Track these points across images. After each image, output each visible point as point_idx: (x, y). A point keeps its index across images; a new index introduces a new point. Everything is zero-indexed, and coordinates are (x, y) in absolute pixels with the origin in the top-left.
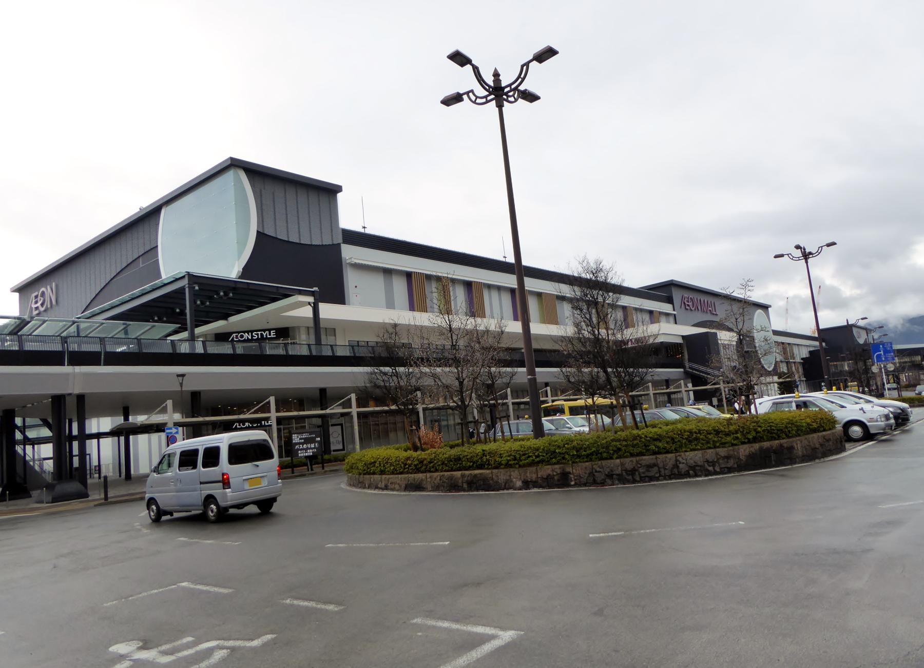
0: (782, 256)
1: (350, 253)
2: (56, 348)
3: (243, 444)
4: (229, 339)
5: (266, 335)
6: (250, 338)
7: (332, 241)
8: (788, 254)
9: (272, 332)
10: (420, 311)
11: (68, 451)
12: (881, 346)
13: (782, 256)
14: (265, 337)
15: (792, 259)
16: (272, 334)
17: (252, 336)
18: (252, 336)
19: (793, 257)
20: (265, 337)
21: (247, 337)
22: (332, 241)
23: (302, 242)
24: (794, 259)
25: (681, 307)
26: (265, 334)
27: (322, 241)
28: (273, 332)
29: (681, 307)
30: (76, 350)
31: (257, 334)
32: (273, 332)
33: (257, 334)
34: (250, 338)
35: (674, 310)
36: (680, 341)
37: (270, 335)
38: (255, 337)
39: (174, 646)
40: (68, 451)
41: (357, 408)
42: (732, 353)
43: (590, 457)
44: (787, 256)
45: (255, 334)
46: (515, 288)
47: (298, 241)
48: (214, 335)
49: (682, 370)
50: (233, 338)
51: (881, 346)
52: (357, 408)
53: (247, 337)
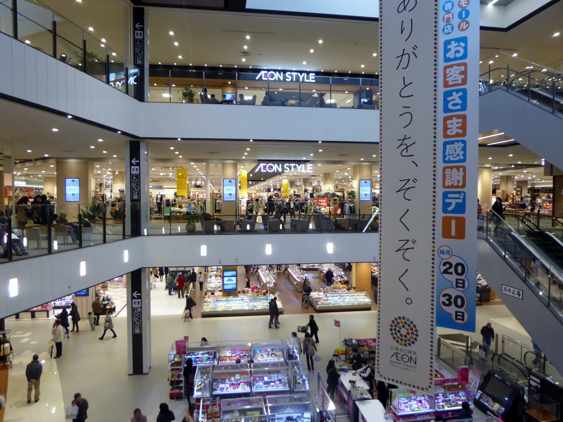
3: (52, 247)
4: (363, 231)
5: (303, 78)
6: (282, 79)
11: (559, 413)
14: (301, 80)
16: (311, 77)
17: (285, 77)
18: (285, 77)
20: (301, 80)
21: (278, 77)
25: (404, 28)
26: (301, 77)
27: (475, 419)
28: (310, 167)
29: (404, 28)
31: (292, 76)
32: (310, 167)
33: (292, 76)
34: (282, 79)
37: (308, 78)
38: (288, 78)
40: (559, 413)
42: (129, 67)
45: (287, 166)
46: (41, 234)
48: (67, 419)
50: (261, 76)
53: (278, 77)
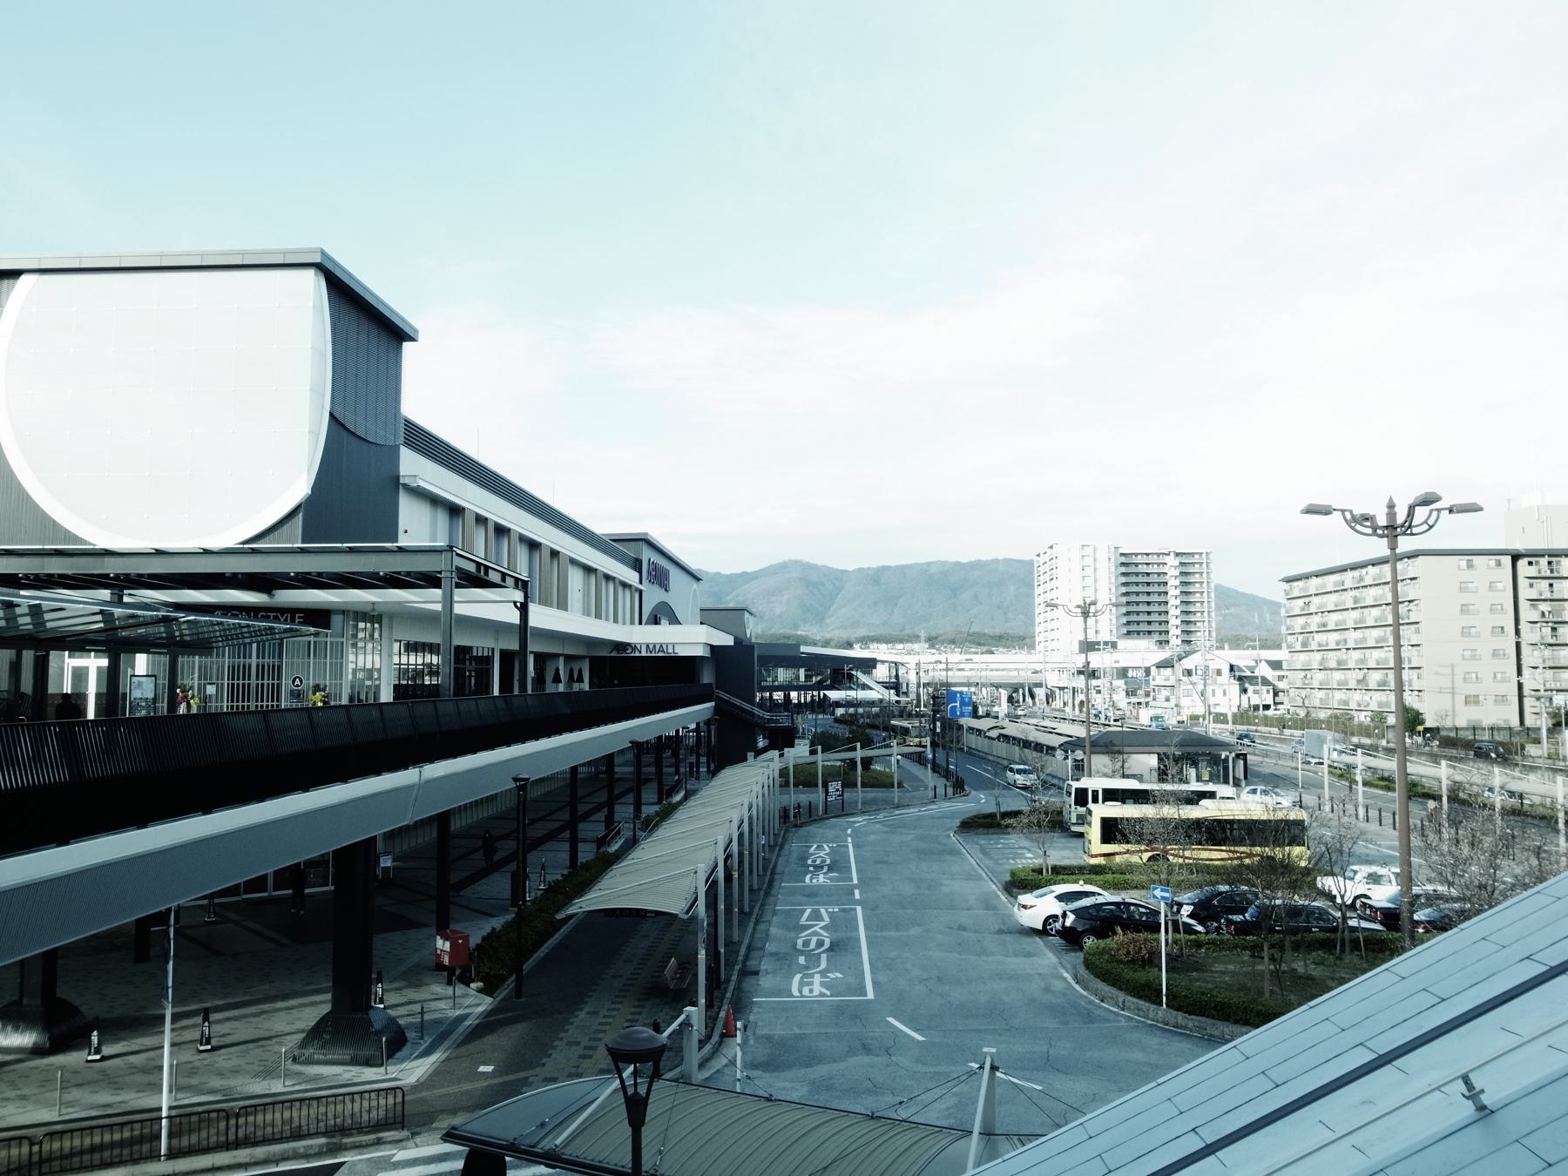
0: (1325, 511)
1: (413, 466)
2: (620, 1099)
7: (1085, 1129)
8: (1343, 511)
9: (297, 615)
10: (607, 620)
12: (958, 695)
13: (1325, 511)
15: (1431, 527)
16: (297, 620)
19: (1426, 522)
22: (1085, 1129)
23: (1213, 1156)
24: (1431, 522)
30: (331, 984)
32: (299, 618)
35: (641, 582)
36: (699, 652)
39: (533, 679)
41: (501, 650)
43: (1079, 754)
44: (1340, 513)
47: (1217, 1154)
49: (713, 704)
51: (958, 695)
52: (501, 650)
